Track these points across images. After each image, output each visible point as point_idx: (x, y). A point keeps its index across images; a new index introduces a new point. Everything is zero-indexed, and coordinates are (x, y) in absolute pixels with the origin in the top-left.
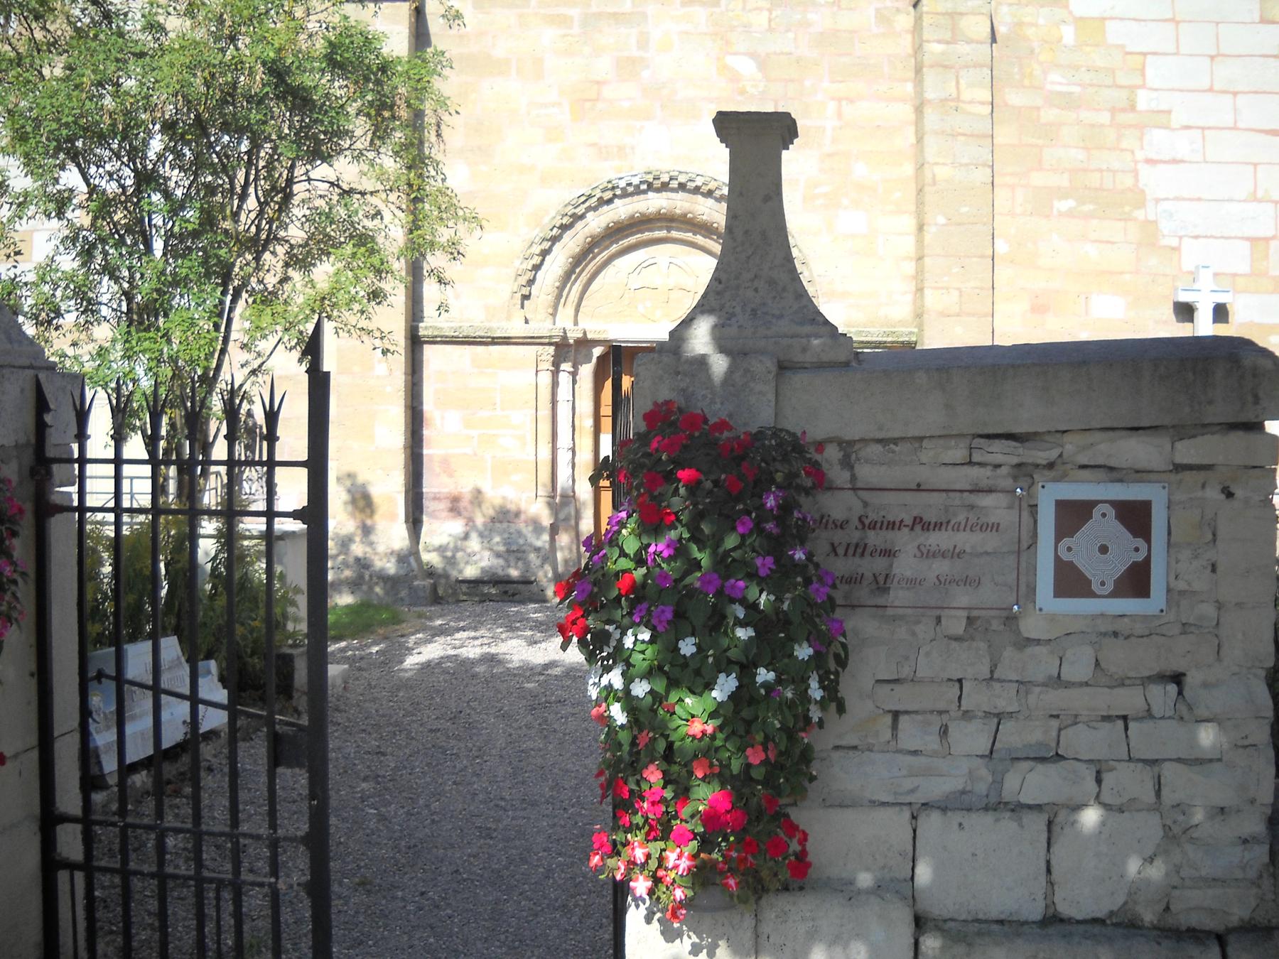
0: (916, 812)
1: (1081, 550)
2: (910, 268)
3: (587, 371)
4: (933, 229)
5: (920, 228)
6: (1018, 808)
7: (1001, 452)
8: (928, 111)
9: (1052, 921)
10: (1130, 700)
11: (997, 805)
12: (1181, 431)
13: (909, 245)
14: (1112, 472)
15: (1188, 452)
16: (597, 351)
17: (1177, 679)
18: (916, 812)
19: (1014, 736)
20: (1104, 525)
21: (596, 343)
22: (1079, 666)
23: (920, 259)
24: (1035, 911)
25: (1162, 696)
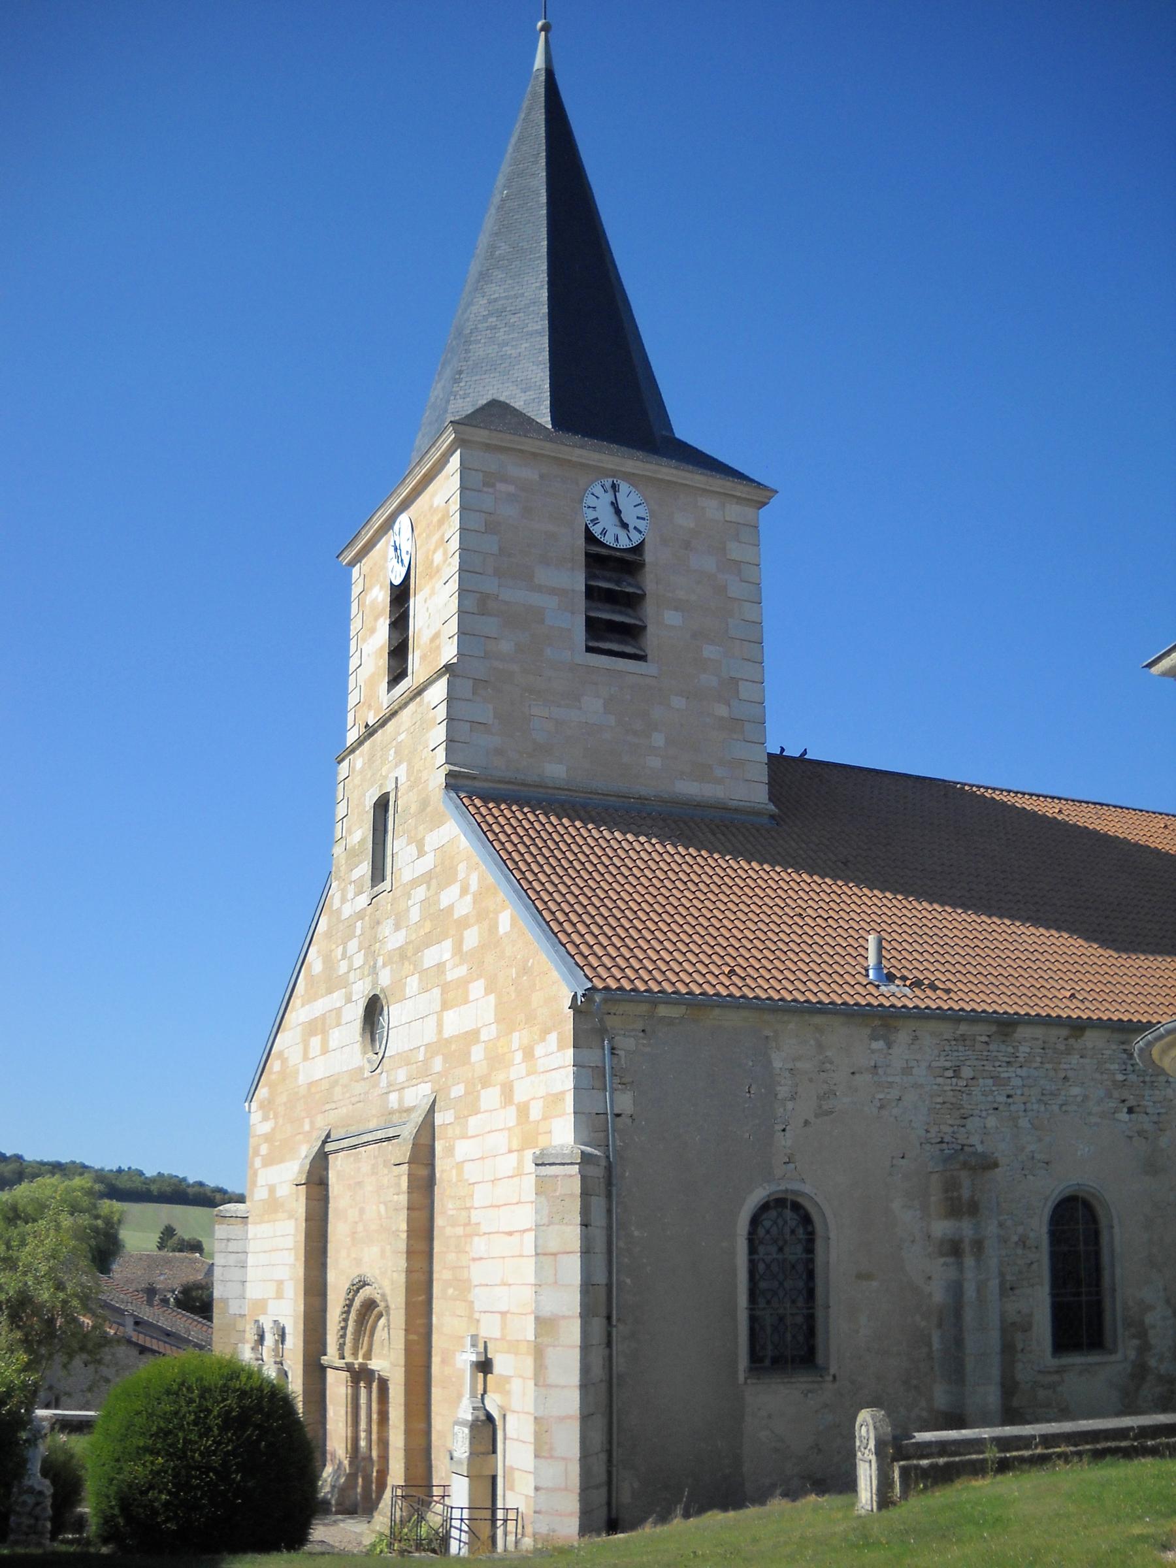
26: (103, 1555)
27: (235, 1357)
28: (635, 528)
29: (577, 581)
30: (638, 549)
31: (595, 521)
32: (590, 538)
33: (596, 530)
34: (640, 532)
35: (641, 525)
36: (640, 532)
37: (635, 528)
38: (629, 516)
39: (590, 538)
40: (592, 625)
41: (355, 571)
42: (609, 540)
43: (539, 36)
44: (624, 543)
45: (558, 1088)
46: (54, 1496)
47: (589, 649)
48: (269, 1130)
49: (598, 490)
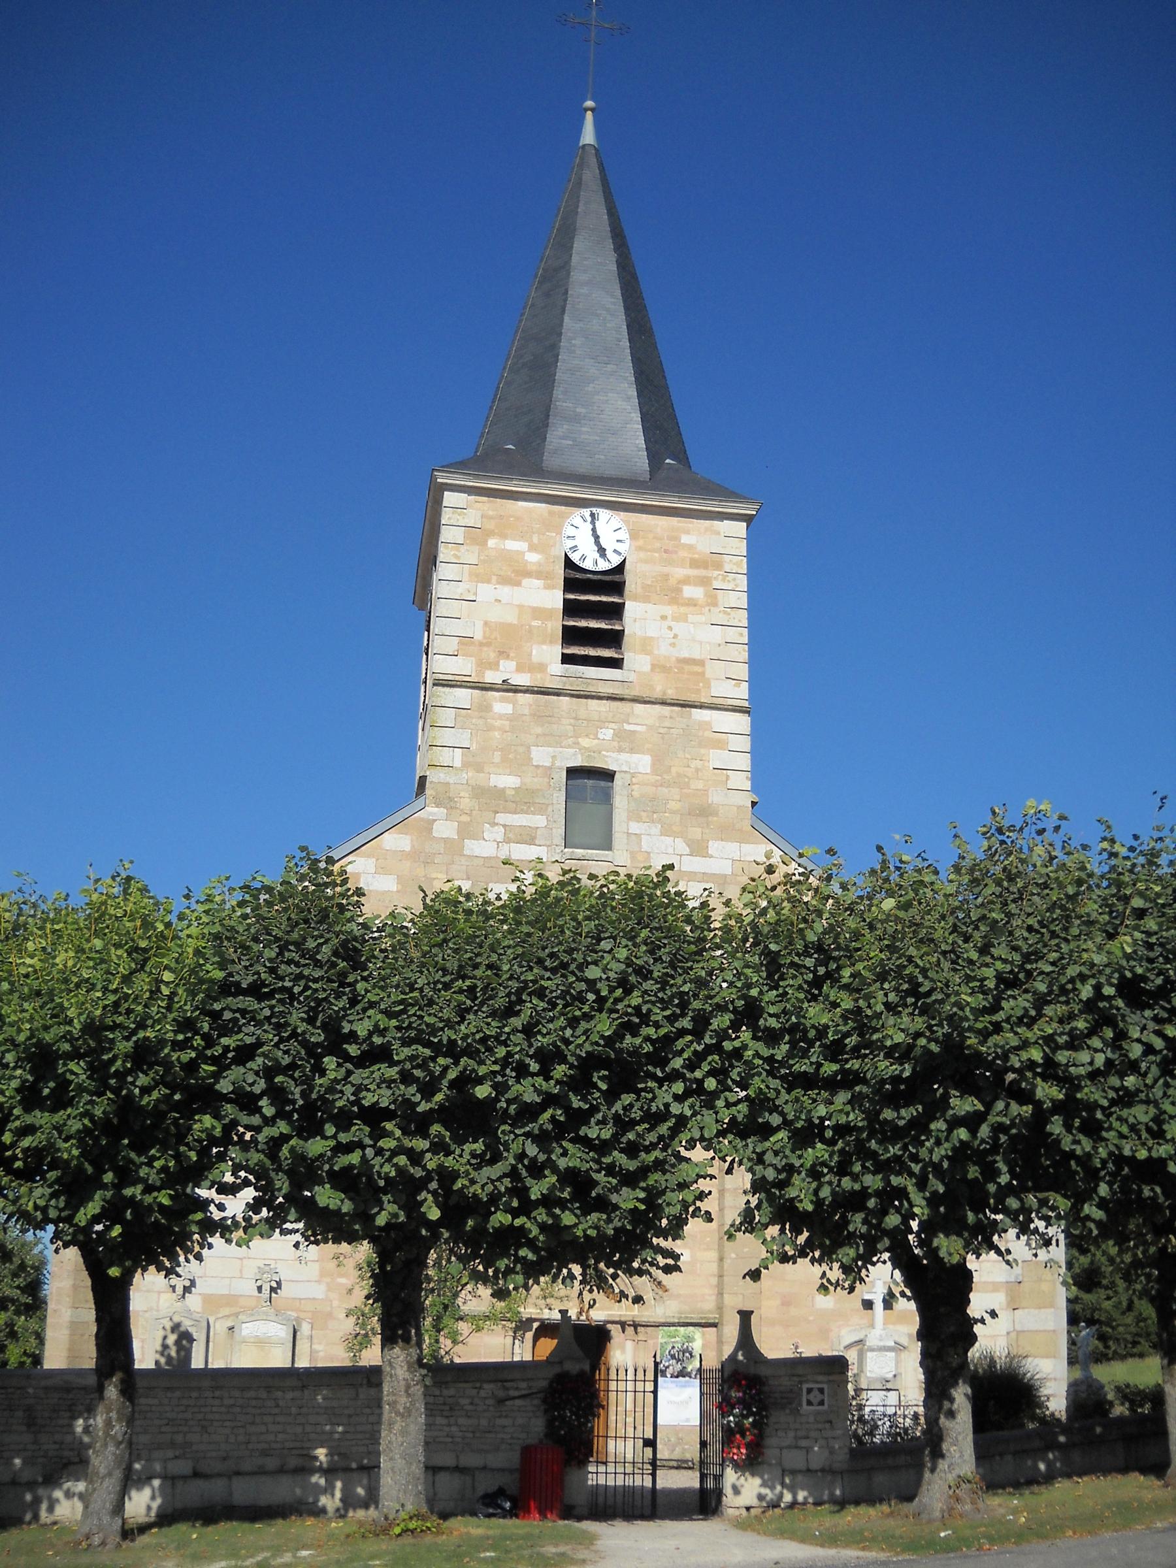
0: (781, 1449)
1: (811, 1397)
2: (714, 1281)
3: (529, 1335)
4: (729, 1261)
5: (721, 1259)
6: (801, 1448)
7: (795, 1379)
8: (727, 1195)
9: (809, 1470)
10: (820, 1426)
11: (796, 1447)
12: (829, 1374)
13: (714, 1268)
14: (817, 1382)
15: (831, 1378)
16: (536, 1325)
17: (831, 1422)
18: (781, 1449)
19: (800, 1433)
20: (816, 1392)
21: (535, 1320)
22: (811, 1419)
23: (721, 1276)
24: (804, 1468)
25: (827, 1426)
26: (78, 1417)
27: (1166, 1362)
28: (615, 551)
29: (555, 598)
30: (620, 569)
31: (574, 549)
32: (569, 564)
33: (575, 558)
34: (619, 554)
35: (621, 548)
36: (619, 554)
37: (615, 551)
38: (607, 542)
39: (569, 564)
40: (570, 636)
41: (152, 1519)
42: (588, 565)
43: (584, 118)
44: (603, 566)
45: (1050, 1326)
46: (926, 1416)
47: (567, 659)
48: (134, 1493)
49: (577, 520)
